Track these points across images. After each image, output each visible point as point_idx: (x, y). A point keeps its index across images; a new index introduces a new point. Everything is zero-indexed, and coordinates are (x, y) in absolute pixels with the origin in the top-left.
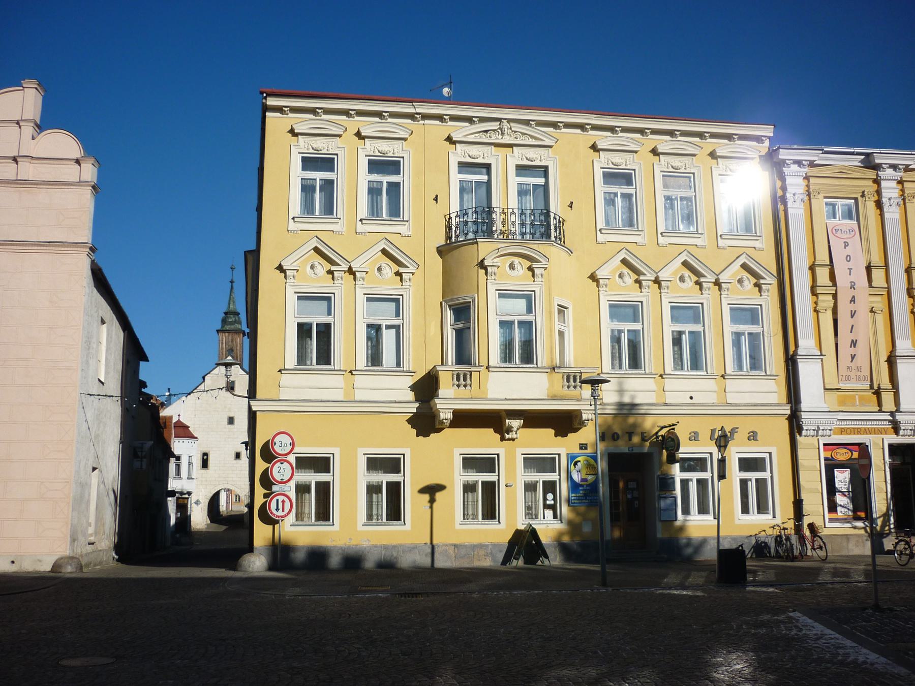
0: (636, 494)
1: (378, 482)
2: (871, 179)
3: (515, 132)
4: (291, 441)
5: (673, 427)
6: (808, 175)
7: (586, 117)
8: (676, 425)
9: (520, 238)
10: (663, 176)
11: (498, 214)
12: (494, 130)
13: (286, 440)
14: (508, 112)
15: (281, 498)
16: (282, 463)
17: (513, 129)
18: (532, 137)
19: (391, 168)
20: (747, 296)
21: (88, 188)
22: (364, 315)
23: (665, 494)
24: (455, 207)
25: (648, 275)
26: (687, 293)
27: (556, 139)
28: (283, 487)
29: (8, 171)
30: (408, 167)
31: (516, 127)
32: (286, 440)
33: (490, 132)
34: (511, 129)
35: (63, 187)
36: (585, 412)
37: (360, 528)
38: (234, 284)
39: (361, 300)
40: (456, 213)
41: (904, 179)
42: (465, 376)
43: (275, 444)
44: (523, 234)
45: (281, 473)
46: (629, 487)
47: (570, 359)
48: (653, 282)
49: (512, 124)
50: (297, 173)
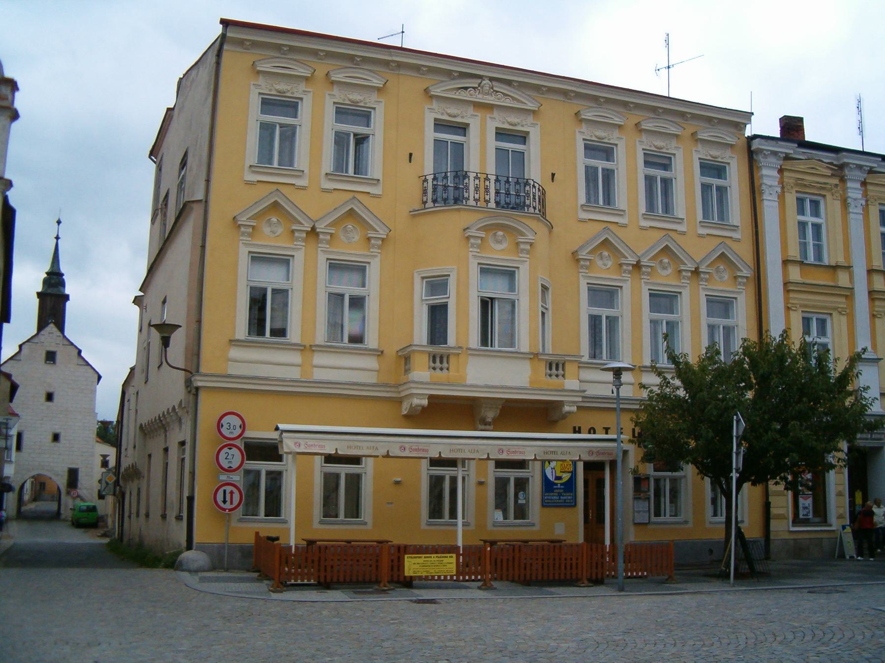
1: (852, 267)
3: (497, 92)
6: (783, 167)
10: (644, 154)
11: (472, 179)
12: (474, 88)
13: (235, 421)
15: (229, 489)
16: (230, 449)
17: (495, 89)
18: (514, 99)
19: (460, 131)
23: (640, 495)
24: (429, 169)
27: (540, 103)
30: (378, 119)
31: (498, 87)
32: (235, 421)
33: (469, 89)
34: (492, 88)
36: (567, 404)
37: (316, 525)
38: (59, 241)
39: (474, 270)
41: (867, 181)
42: (441, 358)
43: (222, 426)
47: (402, 391)
48: (168, 349)
49: (495, 83)
50: (255, 116)
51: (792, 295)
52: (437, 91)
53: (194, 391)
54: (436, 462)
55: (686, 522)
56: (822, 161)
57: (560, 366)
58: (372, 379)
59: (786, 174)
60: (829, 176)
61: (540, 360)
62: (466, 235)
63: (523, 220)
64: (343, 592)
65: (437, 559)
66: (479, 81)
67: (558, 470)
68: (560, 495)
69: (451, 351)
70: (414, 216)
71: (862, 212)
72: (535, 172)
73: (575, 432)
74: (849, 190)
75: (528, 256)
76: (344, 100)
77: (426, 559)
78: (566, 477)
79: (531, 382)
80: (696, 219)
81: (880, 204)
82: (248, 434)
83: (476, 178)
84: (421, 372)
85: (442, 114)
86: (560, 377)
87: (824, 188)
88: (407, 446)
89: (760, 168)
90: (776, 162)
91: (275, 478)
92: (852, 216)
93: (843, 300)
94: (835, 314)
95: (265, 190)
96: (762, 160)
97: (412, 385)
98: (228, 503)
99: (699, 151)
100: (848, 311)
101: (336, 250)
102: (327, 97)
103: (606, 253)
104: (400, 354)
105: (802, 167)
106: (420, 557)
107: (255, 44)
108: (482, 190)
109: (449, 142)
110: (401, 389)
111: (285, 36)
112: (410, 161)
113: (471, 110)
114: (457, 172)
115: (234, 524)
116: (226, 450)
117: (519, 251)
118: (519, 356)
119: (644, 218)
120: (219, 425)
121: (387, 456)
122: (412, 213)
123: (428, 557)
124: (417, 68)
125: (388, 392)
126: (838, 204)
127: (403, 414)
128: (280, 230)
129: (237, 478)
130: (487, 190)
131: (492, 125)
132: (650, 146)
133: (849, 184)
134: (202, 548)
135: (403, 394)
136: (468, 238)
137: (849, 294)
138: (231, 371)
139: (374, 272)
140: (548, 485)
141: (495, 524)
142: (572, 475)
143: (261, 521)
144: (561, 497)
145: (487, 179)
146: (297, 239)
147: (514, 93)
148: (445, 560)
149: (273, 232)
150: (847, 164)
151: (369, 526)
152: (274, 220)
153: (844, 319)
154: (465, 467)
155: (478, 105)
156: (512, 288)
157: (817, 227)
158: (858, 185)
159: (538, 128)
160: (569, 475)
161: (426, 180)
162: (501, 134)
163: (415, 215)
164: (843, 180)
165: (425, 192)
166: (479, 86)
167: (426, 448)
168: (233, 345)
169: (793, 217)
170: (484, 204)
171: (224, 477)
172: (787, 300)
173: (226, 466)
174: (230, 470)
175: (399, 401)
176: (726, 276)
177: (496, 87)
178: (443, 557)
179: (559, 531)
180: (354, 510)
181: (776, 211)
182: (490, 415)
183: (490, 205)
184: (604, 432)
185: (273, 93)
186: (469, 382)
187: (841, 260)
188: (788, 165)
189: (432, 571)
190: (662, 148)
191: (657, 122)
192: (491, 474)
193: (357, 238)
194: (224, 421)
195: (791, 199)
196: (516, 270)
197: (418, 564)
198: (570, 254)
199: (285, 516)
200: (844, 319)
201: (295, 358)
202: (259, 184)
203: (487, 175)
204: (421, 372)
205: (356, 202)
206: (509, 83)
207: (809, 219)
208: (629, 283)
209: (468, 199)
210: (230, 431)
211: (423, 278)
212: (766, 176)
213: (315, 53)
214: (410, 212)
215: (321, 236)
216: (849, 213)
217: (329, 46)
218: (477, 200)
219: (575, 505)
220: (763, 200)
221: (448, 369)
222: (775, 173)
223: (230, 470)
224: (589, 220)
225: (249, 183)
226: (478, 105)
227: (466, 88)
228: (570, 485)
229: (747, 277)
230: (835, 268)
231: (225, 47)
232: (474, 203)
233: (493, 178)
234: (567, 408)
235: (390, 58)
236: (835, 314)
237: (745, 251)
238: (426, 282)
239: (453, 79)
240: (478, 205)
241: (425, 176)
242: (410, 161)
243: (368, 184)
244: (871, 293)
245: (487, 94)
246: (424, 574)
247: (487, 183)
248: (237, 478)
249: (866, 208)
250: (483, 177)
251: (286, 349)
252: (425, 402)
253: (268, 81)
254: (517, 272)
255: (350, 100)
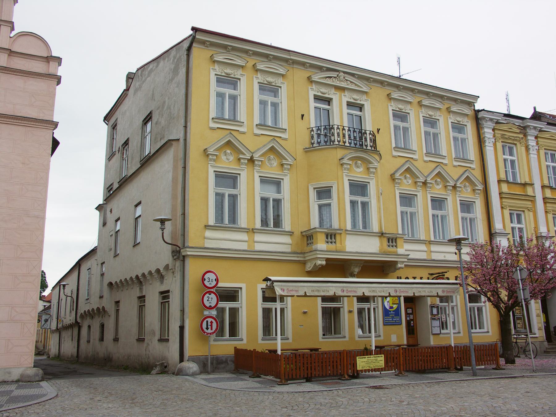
0: (412, 317)
2: (534, 135)
3: (347, 80)
4: (216, 278)
5: (444, 274)
6: (495, 128)
7: (387, 77)
8: (446, 272)
9: (318, 145)
12: (335, 77)
13: (213, 277)
14: (343, 67)
15: (210, 320)
16: (210, 294)
17: (346, 78)
18: (356, 85)
20: (467, 194)
21: (55, 80)
22: (259, 191)
24: (313, 125)
25: (421, 179)
26: (438, 190)
28: (211, 312)
29: (1, 60)
30: (284, 92)
31: (348, 77)
32: (213, 277)
35: (36, 77)
37: (260, 341)
39: (257, 180)
40: (311, 129)
41: (538, 136)
42: (331, 236)
43: (205, 280)
44: (319, 143)
45: (209, 302)
46: (408, 312)
47: (307, 256)
49: (346, 75)
51: (504, 200)
52: (315, 78)
53: (181, 258)
54: (325, 299)
55: (488, 332)
56: (515, 125)
57: (394, 241)
58: (288, 249)
59: (496, 131)
60: (518, 133)
61: (385, 237)
62: (341, 163)
63: (371, 154)
64: (311, 383)
65: (374, 358)
66: (338, 73)
67: (391, 302)
68: (393, 318)
69: (337, 232)
70: (306, 152)
71: (536, 153)
72: (369, 126)
73: (398, 278)
74: (529, 141)
75: (374, 176)
76: (264, 81)
77: (368, 359)
78: (395, 306)
79: (380, 252)
80: (452, 157)
81: (545, 149)
82: (220, 285)
83: (338, 128)
84: (321, 245)
85: (318, 92)
86: (394, 247)
87: (516, 140)
88: (345, 289)
89: (483, 128)
90: (491, 124)
91: (234, 312)
92: (532, 155)
93: (530, 203)
94: (526, 211)
95: (222, 133)
96: (484, 123)
97: (318, 252)
98: (210, 329)
99: (451, 118)
100: (533, 209)
101: (263, 171)
102: (255, 79)
103: (408, 176)
104: (304, 234)
105: (505, 127)
106: (365, 358)
107: (213, 44)
108: (341, 135)
109: (321, 109)
110: (306, 255)
111: (239, 42)
112: (302, 119)
113: (333, 91)
114: (325, 126)
115: (212, 343)
116: (207, 295)
117: (369, 173)
118: (372, 234)
119: (426, 156)
120: (203, 279)
121: (305, 296)
122: (305, 150)
123: (369, 357)
124: (303, 64)
125: (298, 257)
126: (523, 149)
127: (306, 270)
128: (231, 158)
129: (214, 313)
130: (344, 136)
131: (345, 100)
132: (426, 115)
133: (529, 138)
134: (192, 359)
135: (307, 258)
136: (342, 165)
137: (532, 199)
138: (207, 245)
139: (286, 185)
140: (386, 312)
141: (360, 337)
142: (398, 306)
143: (226, 340)
144: (394, 319)
145: (343, 129)
146: (242, 164)
147: (357, 82)
148: (379, 359)
149: (228, 159)
150: (529, 126)
151: (245, 341)
152: (229, 151)
153: (531, 214)
154: (375, 303)
155: (337, 88)
156: (279, 192)
157: (513, 162)
158: (533, 138)
159: (369, 102)
160: (397, 305)
161: (312, 130)
162: (349, 104)
163: (307, 151)
164: (525, 135)
165: (312, 137)
166: (337, 76)
167: (356, 290)
168: (207, 229)
169: (501, 157)
170: (343, 144)
171: (206, 313)
172: (501, 203)
173: (208, 305)
174: (210, 308)
175: (304, 263)
176: (469, 189)
177: (347, 77)
178: (377, 357)
179: (394, 339)
180: (234, 332)
181: (493, 152)
182: (357, 270)
183: (346, 144)
184: (455, 279)
185: (223, 74)
186: (347, 250)
187: (528, 180)
188: (498, 126)
189: (372, 366)
190: (432, 116)
191: (430, 101)
192: (356, 306)
193: (275, 164)
194: (206, 276)
195: (499, 145)
196: (282, 180)
197: (364, 362)
198: (389, 176)
199: (241, 336)
200: (531, 214)
201: (244, 236)
202: (218, 129)
203: (344, 127)
204: (321, 245)
205: (275, 142)
206: (353, 75)
207: (508, 157)
208: (421, 193)
209: (334, 141)
210: (210, 282)
211: (314, 188)
212: (487, 132)
213: (246, 52)
214: (304, 149)
215: (256, 163)
216: (530, 154)
217: (255, 48)
218: (339, 141)
219: (401, 324)
220: (486, 146)
221: (335, 243)
222: (491, 131)
223: (210, 308)
224: (398, 156)
225: (212, 129)
226: (337, 88)
227: (330, 77)
228: (397, 312)
229: (480, 190)
230: (525, 185)
231: (194, 45)
232: (348, 145)
233: (347, 129)
234: (399, 266)
235: (289, 57)
236: (526, 211)
237: (477, 174)
238: (316, 191)
239: (323, 71)
240: (351, 146)
241: (312, 128)
242: (302, 119)
243: (280, 132)
244: (544, 199)
245: (342, 81)
246: (368, 368)
247: (344, 132)
248: (214, 313)
249: (538, 151)
250: (341, 128)
251: (270, 233)
252: (324, 263)
253: (220, 67)
254: (368, 185)
255: (267, 81)
